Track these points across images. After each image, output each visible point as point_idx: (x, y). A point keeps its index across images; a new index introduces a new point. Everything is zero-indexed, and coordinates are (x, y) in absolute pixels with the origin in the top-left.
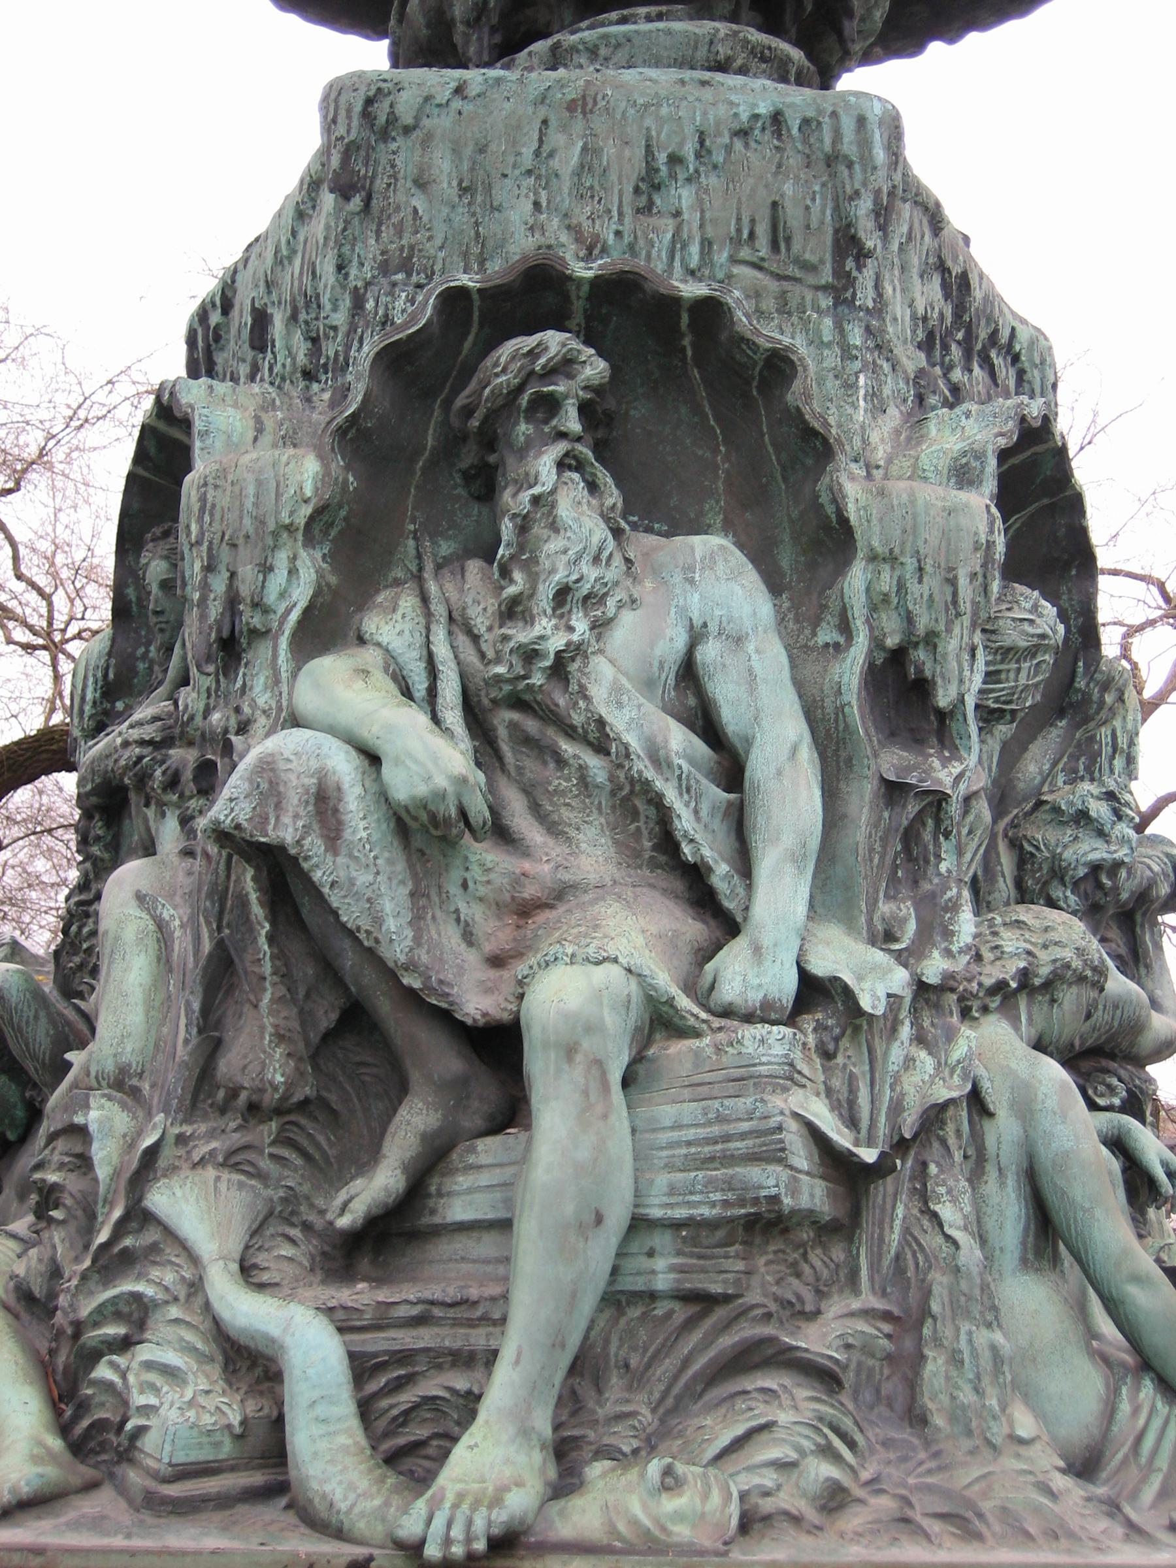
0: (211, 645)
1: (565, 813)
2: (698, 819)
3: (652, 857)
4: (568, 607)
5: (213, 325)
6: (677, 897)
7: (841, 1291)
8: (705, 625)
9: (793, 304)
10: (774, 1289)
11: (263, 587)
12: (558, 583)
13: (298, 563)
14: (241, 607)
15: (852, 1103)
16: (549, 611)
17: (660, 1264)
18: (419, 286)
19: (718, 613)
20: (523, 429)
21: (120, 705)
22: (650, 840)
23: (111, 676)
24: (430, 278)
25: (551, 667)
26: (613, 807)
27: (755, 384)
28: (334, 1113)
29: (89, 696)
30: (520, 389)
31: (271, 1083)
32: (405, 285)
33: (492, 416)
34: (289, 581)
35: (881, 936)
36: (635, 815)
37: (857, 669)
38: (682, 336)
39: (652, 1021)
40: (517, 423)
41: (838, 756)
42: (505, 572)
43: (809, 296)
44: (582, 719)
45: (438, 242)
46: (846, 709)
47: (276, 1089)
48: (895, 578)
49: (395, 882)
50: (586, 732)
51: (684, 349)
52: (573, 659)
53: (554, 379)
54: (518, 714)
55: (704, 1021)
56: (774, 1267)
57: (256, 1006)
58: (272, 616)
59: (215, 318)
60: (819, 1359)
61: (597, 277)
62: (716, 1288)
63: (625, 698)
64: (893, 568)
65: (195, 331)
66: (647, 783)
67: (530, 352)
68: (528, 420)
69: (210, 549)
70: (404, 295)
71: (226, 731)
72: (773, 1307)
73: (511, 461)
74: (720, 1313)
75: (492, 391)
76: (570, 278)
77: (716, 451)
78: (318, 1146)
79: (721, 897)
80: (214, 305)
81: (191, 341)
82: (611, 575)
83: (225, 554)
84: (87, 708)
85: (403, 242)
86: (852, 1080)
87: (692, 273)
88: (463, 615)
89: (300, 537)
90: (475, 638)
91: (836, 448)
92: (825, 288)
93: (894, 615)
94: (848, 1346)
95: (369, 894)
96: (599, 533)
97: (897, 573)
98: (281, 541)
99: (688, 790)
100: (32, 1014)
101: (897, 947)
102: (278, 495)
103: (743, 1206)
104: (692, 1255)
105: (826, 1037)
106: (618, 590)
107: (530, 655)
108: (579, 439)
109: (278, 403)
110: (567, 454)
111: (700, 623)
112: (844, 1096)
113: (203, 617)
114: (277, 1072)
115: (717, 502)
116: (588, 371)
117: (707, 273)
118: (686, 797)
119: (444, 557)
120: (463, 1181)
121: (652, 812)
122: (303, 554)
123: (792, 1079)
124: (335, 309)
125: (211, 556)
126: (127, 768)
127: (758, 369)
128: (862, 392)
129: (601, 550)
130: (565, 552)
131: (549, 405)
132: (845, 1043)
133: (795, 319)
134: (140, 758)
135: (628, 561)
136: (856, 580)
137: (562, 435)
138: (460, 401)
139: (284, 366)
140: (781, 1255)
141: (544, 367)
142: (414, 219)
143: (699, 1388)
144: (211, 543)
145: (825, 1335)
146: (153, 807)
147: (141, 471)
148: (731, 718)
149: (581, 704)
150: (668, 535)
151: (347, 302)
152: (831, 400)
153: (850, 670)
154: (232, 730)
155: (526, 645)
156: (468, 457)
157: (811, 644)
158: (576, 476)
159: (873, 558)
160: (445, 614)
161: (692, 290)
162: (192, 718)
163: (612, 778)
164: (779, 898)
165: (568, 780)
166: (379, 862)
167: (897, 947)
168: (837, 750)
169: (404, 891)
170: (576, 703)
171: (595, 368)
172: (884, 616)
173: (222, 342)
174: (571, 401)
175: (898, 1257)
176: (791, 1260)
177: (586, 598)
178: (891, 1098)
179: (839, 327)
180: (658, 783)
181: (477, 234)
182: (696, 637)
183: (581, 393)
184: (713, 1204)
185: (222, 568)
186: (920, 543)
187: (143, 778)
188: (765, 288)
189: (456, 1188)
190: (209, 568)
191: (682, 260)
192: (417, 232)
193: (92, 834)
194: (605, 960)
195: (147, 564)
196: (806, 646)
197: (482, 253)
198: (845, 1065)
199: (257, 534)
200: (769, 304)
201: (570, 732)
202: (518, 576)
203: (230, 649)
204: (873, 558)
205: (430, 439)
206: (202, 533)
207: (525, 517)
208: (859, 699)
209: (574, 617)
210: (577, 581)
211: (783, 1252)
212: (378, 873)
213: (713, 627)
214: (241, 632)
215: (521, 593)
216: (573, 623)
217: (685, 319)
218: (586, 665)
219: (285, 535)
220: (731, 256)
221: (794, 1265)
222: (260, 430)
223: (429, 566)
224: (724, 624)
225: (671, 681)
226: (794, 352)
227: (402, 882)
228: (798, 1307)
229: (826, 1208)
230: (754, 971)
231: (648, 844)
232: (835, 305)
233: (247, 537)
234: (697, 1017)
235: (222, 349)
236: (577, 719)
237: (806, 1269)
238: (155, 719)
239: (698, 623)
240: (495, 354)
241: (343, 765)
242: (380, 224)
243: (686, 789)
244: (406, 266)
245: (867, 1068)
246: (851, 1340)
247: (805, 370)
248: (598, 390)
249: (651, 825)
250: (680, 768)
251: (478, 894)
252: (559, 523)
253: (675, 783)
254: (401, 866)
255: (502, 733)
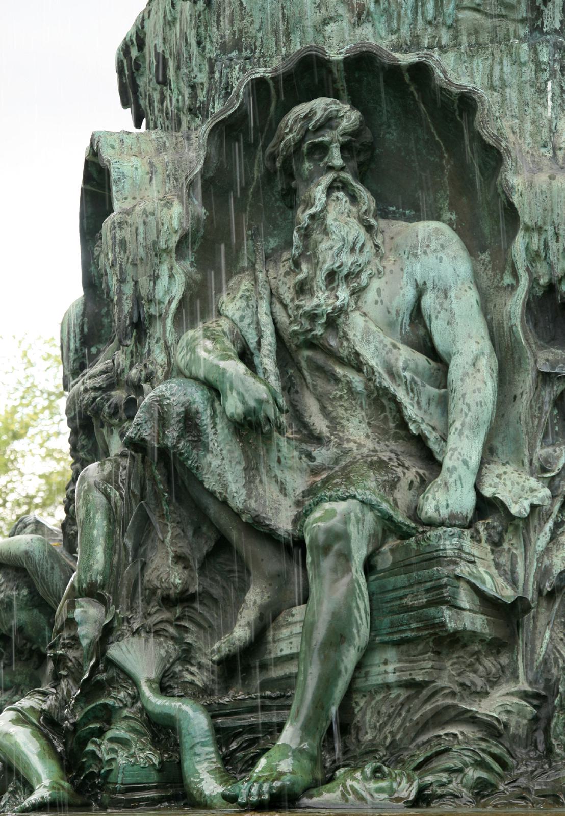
0: (126, 328)
1: (341, 411)
2: (420, 407)
3: (396, 433)
4: (336, 283)
5: (133, 58)
6: (411, 456)
7: (507, 682)
8: (425, 283)
9: (501, 35)
10: (457, 679)
11: (154, 289)
12: (327, 270)
13: (174, 271)
14: (143, 302)
15: (513, 571)
16: (324, 288)
17: (390, 668)
18: (247, 58)
19: (432, 275)
20: (307, 165)
21: (94, 350)
22: (394, 422)
23: (86, 330)
24: (253, 51)
25: (326, 323)
26: (370, 405)
27: (457, 113)
28: (215, 601)
29: (72, 346)
30: (302, 140)
31: (173, 584)
32: (238, 58)
33: (287, 160)
34: (169, 283)
35: (538, 469)
36: (383, 408)
37: (520, 302)
38: (409, 86)
39: (384, 531)
40: (303, 162)
41: (513, 358)
42: (297, 264)
43: (512, 27)
44: (346, 353)
45: (257, 26)
46: (514, 329)
47: (176, 587)
48: (542, 240)
49: (233, 463)
50: (349, 360)
51: (412, 93)
52: (339, 317)
53: (322, 132)
54: (307, 352)
55: (413, 528)
56: (456, 666)
57: (163, 542)
58: (162, 306)
59: (134, 53)
60: (485, 717)
61: (345, 59)
62: (419, 678)
63: (371, 337)
64: (540, 234)
65: (122, 61)
66: (386, 390)
67: (306, 116)
68: (310, 159)
69: (121, 268)
70: (237, 67)
71: (140, 380)
72: (457, 689)
73: (301, 187)
74: (425, 692)
75: (285, 145)
76: (329, 61)
77: (442, 157)
78: (206, 619)
79: (435, 454)
80: (131, 41)
81: (120, 71)
82: (362, 259)
83: (130, 270)
84: (72, 354)
85: (235, 28)
86: (513, 558)
87: (430, 23)
88: (277, 292)
89: (174, 255)
90: (285, 307)
91: (505, 155)
92: (523, 21)
93: (544, 264)
94: (508, 712)
95: (219, 471)
96: (355, 231)
97: (543, 237)
98: (163, 259)
99: (412, 391)
100: (49, 566)
101: (548, 475)
102: (158, 232)
103: (426, 630)
104: (406, 662)
105: (492, 532)
106: (369, 267)
107: (312, 317)
108: (342, 169)
109: (167, 144)
110: (335, 180)
111: (422, 282)
112: (508, 568)
113: (121, 311)
114: (176, 578)
115: (445, 192)
116: (344, 124)
117: (441, 20)
118: (411, 395)
119: (272, 249)
120: (285, 632)
121: (393, 406)
122: (177, 266)
123: (461, 558)
124: (201, 71)
125: (122, 273)
126: (87, 405)
127: (456, 105)
128: (550, 95)
129: (354, 244)
130: (332, 248)
131: (322, 149)
132: (507, 537)
133: (503, 47)
134: (95, 399)
135: (377, 246)
136: (520, 242)
137: (331, 168)
138: (269, 150)
139: (178, 101)
140: (461, 660)
141: (314, 127)
142: (241, 10)
143: (412, 735)
144: (121, 265)
145: (491, 705)
146: (106, 428)
147: (88, 187)
148: (440, 341)
149: (345, 344)
150: (410, 219)
151: (206, 68)
152: (528, 104)
153: (514, 306)
154: (143, 378)
155: (309, 312)
156: (280, 184)
157: (500, 285)
158: (341, 194)
159: (527, 229)
160: (267, 292)
161: (406, 59)
162: (123, 371)
163: (366, 387)
164: (462, 450)
165: (341, 390)
166: (224, 452)
167: (548, 475)
168: (512, 354)
169: (240, 468)
170: (342, 344)
171: (349, 117)
172: (539, 265)
173: (141, 69)
174: (334, 145)
175: (545, 661)
176: (468, 662)
177: (347, 276)
178: (538, 567)
179: (534, 49)
180: (392, 389)
181: (283, 14)
182: (420, 293)
183: (341, 139)
184: (412, 630)
185: (129, 279)
186: (555, 216)
187: (98, 411)
188: (482, 26)
189: (282, 636)
190: (122, 281)
191: (423, 13)
192: (243, 19)
193: (79, 444)
194: (348, 497)
195: (99, 255)
196: (497, 286)
197: (287, 28)
198: (509, 549)
199: (147, 256)
200: (484, 38)
201: (341, 361)
202: (304, 267)
203: (140, 327)
204: (527, 229)
205: (256, 173)
206: (115, 259)
207: (307, 228)
208: (522, 321)
209: (340, 289)
210: (339, 267)
211: (462, 657)
212: (223, 459)
213: (430, 285)
214: (144, 318)
215: (306, 278)
216: (338, 293)
217: (407, 77)
218: (347, 319)
219: (165, 255)
220: (457, 5)
221: (471, 665)
222: (152, 173)
223: (260, 256)
224: (436, 281)
225: (407, 320)
226: (475, 93)
227: (239, 463)
228: (473, 689)
229: (487, 631)
230: (451, 496)
231: (392, 425)
232: (531, 32)
233: (142, 259)
234: (408, 526)
235: (142, 75)
236: (344, 353)
237: (481, 668)
238: (103, 372)
239: (420, 282)
240: (286, 118)
241: (197, 397)
242: (219, 16)
243: (411, 388)
244: (237, 45)
245: (523, 550)
246: (509, 708)
247: (483, 104)
248: (355, 134)
249: (394, 413)
250: (405, 377)
251: (288, 465)
252: (329, 230)
253: (404, 387)
254: (237, 453)
255: (304, 364)
